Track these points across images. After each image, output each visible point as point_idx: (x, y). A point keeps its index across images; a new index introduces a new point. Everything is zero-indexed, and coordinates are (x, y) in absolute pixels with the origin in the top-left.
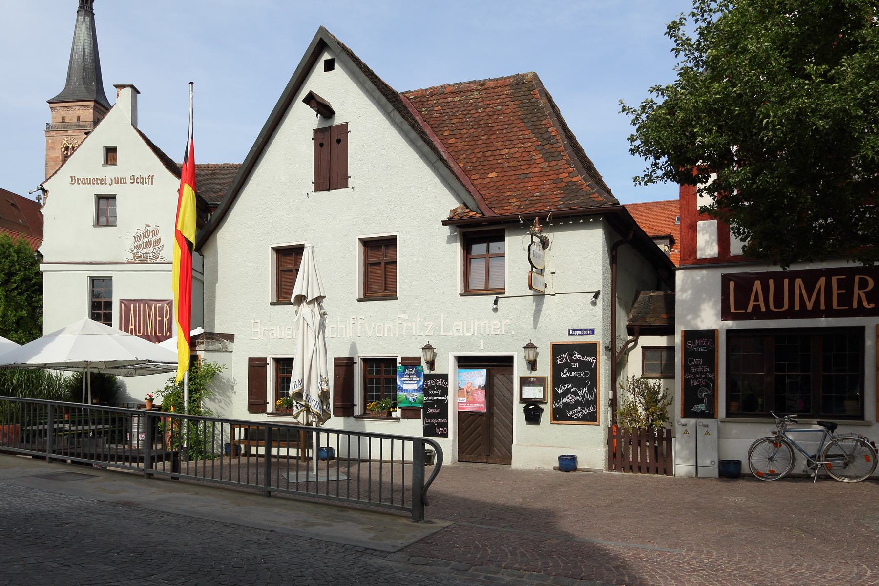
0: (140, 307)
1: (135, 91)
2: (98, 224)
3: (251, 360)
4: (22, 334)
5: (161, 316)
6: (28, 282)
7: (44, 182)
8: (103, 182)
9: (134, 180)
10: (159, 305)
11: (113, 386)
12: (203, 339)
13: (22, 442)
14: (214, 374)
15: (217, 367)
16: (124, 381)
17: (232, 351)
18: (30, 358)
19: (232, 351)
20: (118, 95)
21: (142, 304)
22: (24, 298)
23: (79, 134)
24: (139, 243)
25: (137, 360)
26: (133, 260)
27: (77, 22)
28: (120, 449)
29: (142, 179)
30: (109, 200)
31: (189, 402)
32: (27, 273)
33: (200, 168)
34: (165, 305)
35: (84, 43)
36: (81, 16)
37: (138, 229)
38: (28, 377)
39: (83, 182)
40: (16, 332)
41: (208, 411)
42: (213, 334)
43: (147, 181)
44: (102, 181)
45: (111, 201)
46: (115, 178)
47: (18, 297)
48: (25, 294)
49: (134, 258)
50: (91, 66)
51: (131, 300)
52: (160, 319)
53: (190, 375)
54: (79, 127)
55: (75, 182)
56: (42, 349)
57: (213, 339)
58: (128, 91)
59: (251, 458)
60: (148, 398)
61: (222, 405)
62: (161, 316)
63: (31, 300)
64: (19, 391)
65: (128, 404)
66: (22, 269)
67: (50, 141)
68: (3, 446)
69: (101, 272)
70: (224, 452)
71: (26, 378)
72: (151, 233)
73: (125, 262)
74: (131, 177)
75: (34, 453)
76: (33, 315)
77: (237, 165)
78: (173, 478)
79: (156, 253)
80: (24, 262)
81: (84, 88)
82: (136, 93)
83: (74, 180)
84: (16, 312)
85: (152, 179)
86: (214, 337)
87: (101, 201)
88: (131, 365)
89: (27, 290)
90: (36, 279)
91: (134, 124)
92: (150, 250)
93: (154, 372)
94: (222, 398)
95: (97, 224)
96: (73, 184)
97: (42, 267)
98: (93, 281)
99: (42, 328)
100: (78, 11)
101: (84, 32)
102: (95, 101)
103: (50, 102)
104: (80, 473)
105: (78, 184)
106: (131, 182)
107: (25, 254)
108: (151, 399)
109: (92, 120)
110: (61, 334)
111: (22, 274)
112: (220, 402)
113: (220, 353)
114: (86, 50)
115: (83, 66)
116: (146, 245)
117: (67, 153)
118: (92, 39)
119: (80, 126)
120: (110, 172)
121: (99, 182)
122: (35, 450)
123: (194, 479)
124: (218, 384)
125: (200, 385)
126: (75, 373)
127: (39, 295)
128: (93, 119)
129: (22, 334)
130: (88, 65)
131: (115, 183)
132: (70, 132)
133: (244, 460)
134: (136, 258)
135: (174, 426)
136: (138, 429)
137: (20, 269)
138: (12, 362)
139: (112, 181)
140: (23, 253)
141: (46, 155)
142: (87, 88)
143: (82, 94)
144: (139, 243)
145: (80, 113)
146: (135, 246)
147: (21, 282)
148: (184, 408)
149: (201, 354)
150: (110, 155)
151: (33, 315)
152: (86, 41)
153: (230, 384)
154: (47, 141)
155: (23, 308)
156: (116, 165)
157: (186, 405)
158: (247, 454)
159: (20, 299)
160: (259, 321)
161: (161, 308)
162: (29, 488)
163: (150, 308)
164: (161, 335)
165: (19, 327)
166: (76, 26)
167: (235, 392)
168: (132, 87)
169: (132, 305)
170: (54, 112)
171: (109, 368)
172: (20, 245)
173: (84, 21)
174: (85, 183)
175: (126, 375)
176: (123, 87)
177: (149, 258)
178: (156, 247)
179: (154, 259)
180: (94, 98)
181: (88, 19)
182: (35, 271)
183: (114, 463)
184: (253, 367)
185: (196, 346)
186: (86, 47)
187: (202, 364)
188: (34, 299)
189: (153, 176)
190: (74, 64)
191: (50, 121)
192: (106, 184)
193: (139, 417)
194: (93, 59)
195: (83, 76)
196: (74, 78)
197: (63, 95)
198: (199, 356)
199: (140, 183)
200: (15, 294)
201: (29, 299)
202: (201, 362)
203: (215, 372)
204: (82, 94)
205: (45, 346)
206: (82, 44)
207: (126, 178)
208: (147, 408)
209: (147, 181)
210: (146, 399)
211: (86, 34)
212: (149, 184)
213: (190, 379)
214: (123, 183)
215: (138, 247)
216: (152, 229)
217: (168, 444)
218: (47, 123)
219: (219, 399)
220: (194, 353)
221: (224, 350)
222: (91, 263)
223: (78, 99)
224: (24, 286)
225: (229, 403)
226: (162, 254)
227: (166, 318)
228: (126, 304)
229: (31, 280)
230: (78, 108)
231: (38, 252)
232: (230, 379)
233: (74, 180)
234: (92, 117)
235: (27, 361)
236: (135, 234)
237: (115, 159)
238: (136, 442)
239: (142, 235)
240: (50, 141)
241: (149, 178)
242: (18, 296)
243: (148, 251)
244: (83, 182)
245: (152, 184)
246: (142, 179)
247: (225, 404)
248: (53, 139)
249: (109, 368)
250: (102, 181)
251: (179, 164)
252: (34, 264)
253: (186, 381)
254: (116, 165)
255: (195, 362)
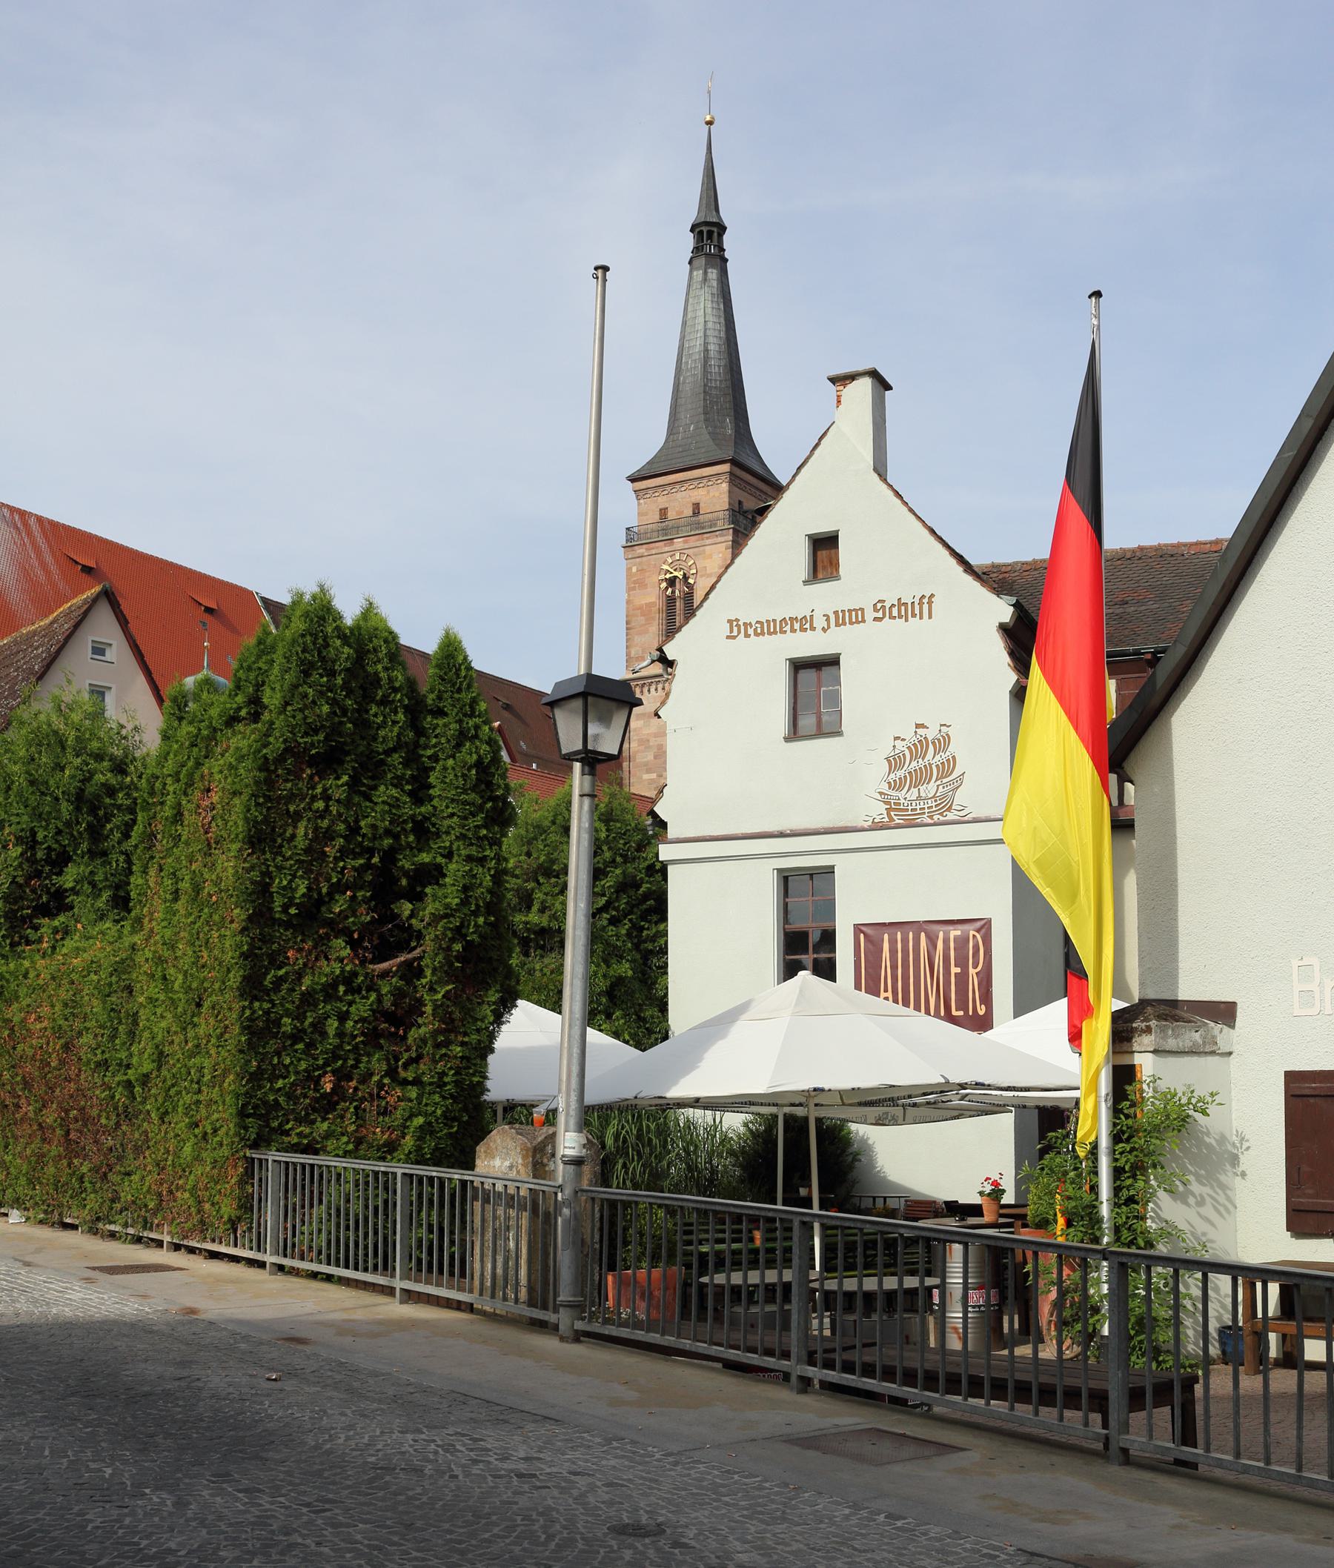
0: (905, 941)
1: (882, 384)
2: (795, 733)
3: (1291, 1077)
4: (622, 1021)
5: (962, 962)
6: (632, 892)
7: (665, 642)
8: (807, 626)
9: (883, 611)
10: (955, 932)
11: (844, 1151)
12: (1147, 1020)
13: (685, 1314)
14: (1184, 1119)
15: (1194, 1101)
16: (868, 1138)
17: (1230, 1053)
18: (675, 1082)
19: (1230, 1053)
20: (839, 402)
21: (911, 934)
22: (624, 932)
23: (698, 544)
24: (901, 773)
25: (947, 1082)
26: (887, 819)
27: (689, 286)
28: (1001, 1358)
29: (903, 608)
30: (820, 670)
31: (1115, 1204)
32: (630, 869)
33: (1036, 570)
34: (972, 933)
35: (705, 330)
36: (697, 269)
37: (896, 738)
38: (640, 1130)
39: (759, 631)
40: (609, 1016)
41: (1169, 1232)
42: (1174, 1004)
43: (917, 611)
44: (805, 624)
45: (827, 671)
46: (836, 613)
47: (611, 930)
48: (626, 921)
49: (889, 815)
50: (721, 381)
51: (884, 924)
52: (958, 970)
53: (1115, 1125)
54: (697, 529)
55: (739, 632)
56: (700, 1059)
57: (1176, 1019)
58: (865, 384)
59: (1310, 1376)
60: (988, 1188)
61: (1208, 1210)
62: (962, 962)
63: (639, 936)
64: (619, 1166)
65: (885, 1198)
66: (619, 859)
67: (634, 569)
68: (648, 1331)
69: (805, 854)
70: (1214, 1351)
71: (635, 1132)
72: (931, 747)
73: (866, 825)
74: (875, 605)
75: (733, 1354)
76: (644, 973)
77: (1133, 551)
78: (1178, 1462)
79: (944, 796)
80: (622, 841)
81: (708, 437)
82: (882, 389)
83: (735, 629)
84: (608, 966)
85: (930, 603)
86: (1178, 1012)
87: (803, 675)
88: (910, 1097)
89: (631, 913)
90: (650, 883)
91: (880, 470)
92: (930, 789)
93: (956, 1113)
94: (1206, 1190)
95: (794, 733)
96: (734, 637)
97: (665, 852)
98: (786, 878)
99: (666, 1004)
100: (691, 258)
101: (705, 306)
102: (734, 462)
103: (633, 479)
104: (904, 1435)
105: (747, 636)
106: (875, 619)
107: (623, 822)
108: (997, 1193)
109: (727, 507)
110: (744, 1017)
111: (618, 871)
112: (1201, 1203)
113: (1195, 1059)
114: (711, 347)
115: (705, 385)
116: (919, 778)
117: (673, 592)
118: (722, 320)
119: (699, 525)
120: (825, 597)
121: (797, 626)
122: (738, 1348)
123: (1298, 1480)
124: (1194, 1150)
125: (1149, 1154)
126: (750, 1117)
127: (656, 923)
128: (730, 504)
129: (622, 1021)
130: (716, 380)
131: (837, 625)
132: (679, 543)
133: (1283, 1381)
134: (892, 813)
135: (1066, 1271)
136: (965, 1277)
137: (614, 861)
138: (630, 1095)
139: (828, 620)
140: (618, 821)
141: (628, 602)
142: (714, 435)
143: (703, 450)
144: (901, 773)
145: (699, 494)
146: (889, 783)
147: (617, 892)
148: (1100, 1221)
149: (1145, 1063)
150: (823, 554)
151: (644, 973)
152: (710, 325)
153: (1227, 1151)
154: (629, 569)
155: (622, 957)
156: (837, 578)
157: (1105, 1210)
158: (1292, 1359)
159: (616, 935)
160: (1315, 961)
161: (962, 942)
162: (786, 1485)
163: (932, 942)
164: (961, 1013)
165: (615, 1004)
166: (688, 294)
167: (1243, 1174)
168: (874, 374)
169: (886, 937)
170: (642, 501)
171: (851, 1105)
172: (610, 802)
173: (705, 279)
174: (762, 633)
175: (879, 1122)
176: (852, 377)
177: (926, 811)
178: (945, 781)
179: (941, 814)
180: (729, 454)
181: (713, 274)
182: (647, 863)
183: (982, 1402)
184: (1299, 1100)
185: (1129, 1040)
186: (711, 340)
187: (1148, 1093)
188: (645, 933)
189: (932, 595)
190: (684, 383)
191: (633, 522)
192: (813, 629)
193: (966, 1245)
194: (725, 366)
195: (705, 407)
196: (685, 417)
197: (663, 458)
198: (1138, 1068)
199: (900, 617)
200: (605, 923)
201: (635, 934)
202: (1145, 1087)
203: (1188, 1116)
204: (703, 450)
205: (706, 1050)
206: (701, 334)
207: (862, 610)
208: (987, 1218)
209: (917, 611)
210: (981, 1193)
211: (709, 311)
212: (921, 618)
213: (1116, 1138)
214: (857, 622)
215: (896, 785)
216: (931, 734)
217: (1049, 1329)
218: (628, 529)
219: (1197, 1194)
220: (1124, 1060)
221: (1207, 1050)
222: (782, 835)
223: (695, 463)
224: (623, 903)
225: (1227, 1207)
226: (960, 798)
227: (975, 966)
228: (869, 934)
229: (638, 886)
230: (696, 483)
231: (653, 814)
232: (1228, 1136)
233: (737, 628)
234: (727, 500)
235: (668, 1089)
236: (888, 751)
237: (834, 564)
238: (961, 1315)
239: (907, 753)
240: (634, 569)
241: (921, 604)
242: (611, 928)
243: (923, 794)
244: (759, 631)
245: (930, 617)
246: (903, 608)
247: (1214, 1207)
248: (640, 563)
249: (851, 1105)
250: (805, 624)
251: (978, 566)
252: (645, 847)
253: (1104, 1143)
254: (837, 578)
255: (1128, 1087)
